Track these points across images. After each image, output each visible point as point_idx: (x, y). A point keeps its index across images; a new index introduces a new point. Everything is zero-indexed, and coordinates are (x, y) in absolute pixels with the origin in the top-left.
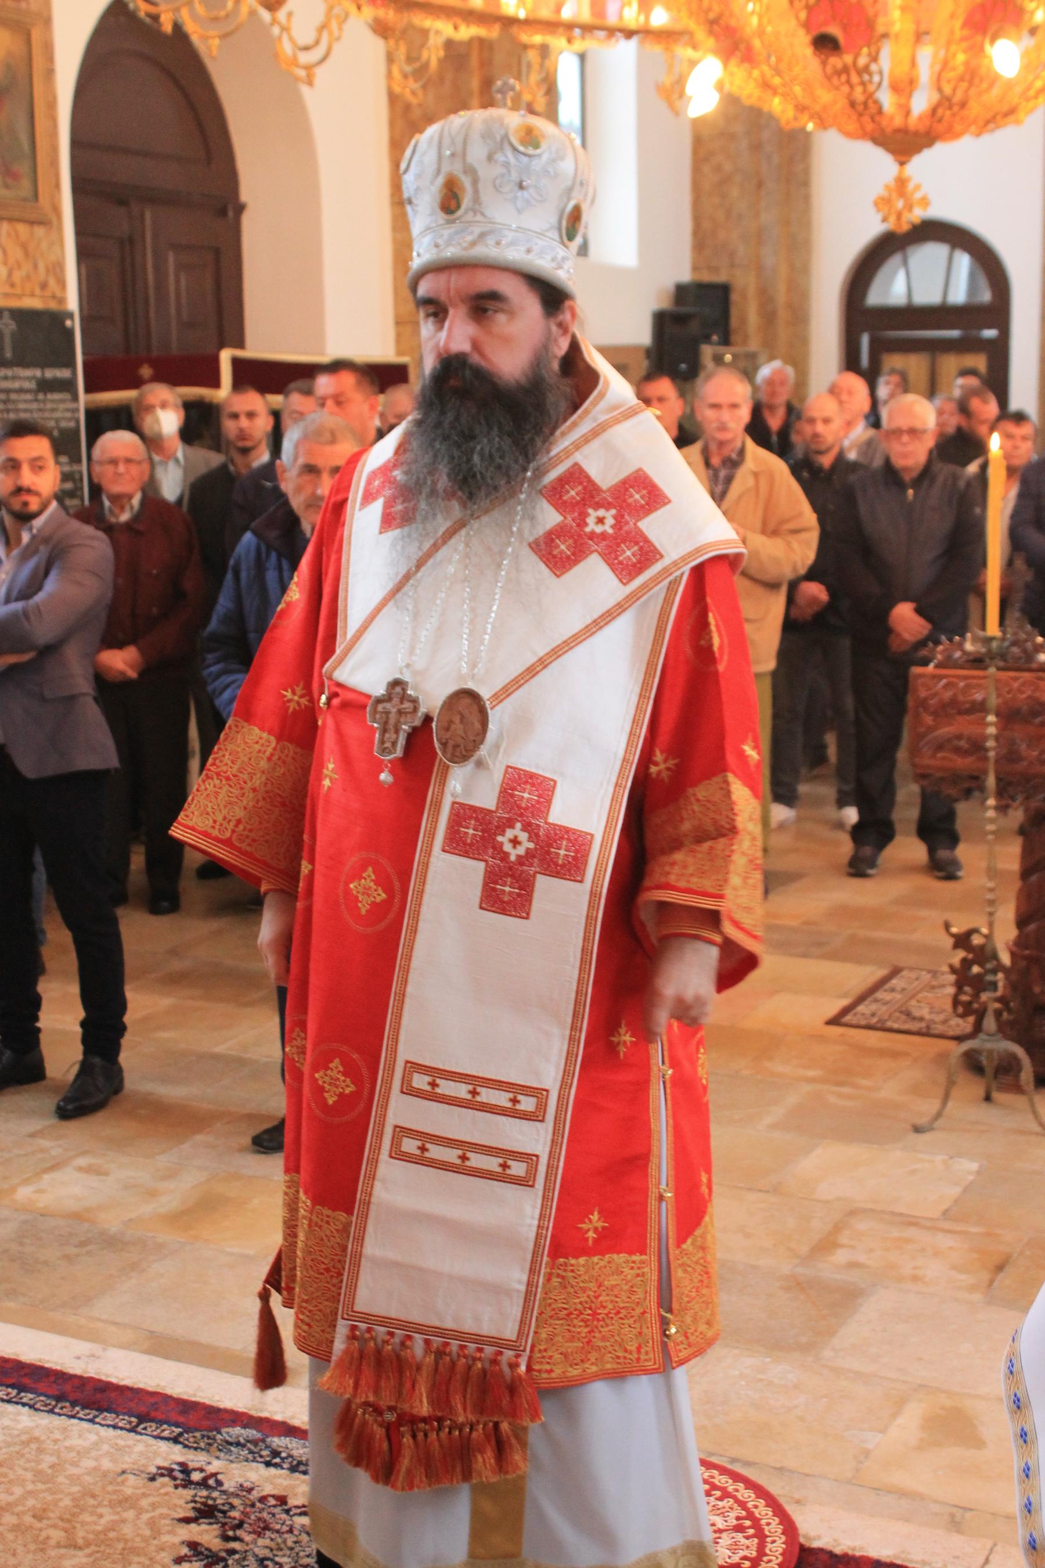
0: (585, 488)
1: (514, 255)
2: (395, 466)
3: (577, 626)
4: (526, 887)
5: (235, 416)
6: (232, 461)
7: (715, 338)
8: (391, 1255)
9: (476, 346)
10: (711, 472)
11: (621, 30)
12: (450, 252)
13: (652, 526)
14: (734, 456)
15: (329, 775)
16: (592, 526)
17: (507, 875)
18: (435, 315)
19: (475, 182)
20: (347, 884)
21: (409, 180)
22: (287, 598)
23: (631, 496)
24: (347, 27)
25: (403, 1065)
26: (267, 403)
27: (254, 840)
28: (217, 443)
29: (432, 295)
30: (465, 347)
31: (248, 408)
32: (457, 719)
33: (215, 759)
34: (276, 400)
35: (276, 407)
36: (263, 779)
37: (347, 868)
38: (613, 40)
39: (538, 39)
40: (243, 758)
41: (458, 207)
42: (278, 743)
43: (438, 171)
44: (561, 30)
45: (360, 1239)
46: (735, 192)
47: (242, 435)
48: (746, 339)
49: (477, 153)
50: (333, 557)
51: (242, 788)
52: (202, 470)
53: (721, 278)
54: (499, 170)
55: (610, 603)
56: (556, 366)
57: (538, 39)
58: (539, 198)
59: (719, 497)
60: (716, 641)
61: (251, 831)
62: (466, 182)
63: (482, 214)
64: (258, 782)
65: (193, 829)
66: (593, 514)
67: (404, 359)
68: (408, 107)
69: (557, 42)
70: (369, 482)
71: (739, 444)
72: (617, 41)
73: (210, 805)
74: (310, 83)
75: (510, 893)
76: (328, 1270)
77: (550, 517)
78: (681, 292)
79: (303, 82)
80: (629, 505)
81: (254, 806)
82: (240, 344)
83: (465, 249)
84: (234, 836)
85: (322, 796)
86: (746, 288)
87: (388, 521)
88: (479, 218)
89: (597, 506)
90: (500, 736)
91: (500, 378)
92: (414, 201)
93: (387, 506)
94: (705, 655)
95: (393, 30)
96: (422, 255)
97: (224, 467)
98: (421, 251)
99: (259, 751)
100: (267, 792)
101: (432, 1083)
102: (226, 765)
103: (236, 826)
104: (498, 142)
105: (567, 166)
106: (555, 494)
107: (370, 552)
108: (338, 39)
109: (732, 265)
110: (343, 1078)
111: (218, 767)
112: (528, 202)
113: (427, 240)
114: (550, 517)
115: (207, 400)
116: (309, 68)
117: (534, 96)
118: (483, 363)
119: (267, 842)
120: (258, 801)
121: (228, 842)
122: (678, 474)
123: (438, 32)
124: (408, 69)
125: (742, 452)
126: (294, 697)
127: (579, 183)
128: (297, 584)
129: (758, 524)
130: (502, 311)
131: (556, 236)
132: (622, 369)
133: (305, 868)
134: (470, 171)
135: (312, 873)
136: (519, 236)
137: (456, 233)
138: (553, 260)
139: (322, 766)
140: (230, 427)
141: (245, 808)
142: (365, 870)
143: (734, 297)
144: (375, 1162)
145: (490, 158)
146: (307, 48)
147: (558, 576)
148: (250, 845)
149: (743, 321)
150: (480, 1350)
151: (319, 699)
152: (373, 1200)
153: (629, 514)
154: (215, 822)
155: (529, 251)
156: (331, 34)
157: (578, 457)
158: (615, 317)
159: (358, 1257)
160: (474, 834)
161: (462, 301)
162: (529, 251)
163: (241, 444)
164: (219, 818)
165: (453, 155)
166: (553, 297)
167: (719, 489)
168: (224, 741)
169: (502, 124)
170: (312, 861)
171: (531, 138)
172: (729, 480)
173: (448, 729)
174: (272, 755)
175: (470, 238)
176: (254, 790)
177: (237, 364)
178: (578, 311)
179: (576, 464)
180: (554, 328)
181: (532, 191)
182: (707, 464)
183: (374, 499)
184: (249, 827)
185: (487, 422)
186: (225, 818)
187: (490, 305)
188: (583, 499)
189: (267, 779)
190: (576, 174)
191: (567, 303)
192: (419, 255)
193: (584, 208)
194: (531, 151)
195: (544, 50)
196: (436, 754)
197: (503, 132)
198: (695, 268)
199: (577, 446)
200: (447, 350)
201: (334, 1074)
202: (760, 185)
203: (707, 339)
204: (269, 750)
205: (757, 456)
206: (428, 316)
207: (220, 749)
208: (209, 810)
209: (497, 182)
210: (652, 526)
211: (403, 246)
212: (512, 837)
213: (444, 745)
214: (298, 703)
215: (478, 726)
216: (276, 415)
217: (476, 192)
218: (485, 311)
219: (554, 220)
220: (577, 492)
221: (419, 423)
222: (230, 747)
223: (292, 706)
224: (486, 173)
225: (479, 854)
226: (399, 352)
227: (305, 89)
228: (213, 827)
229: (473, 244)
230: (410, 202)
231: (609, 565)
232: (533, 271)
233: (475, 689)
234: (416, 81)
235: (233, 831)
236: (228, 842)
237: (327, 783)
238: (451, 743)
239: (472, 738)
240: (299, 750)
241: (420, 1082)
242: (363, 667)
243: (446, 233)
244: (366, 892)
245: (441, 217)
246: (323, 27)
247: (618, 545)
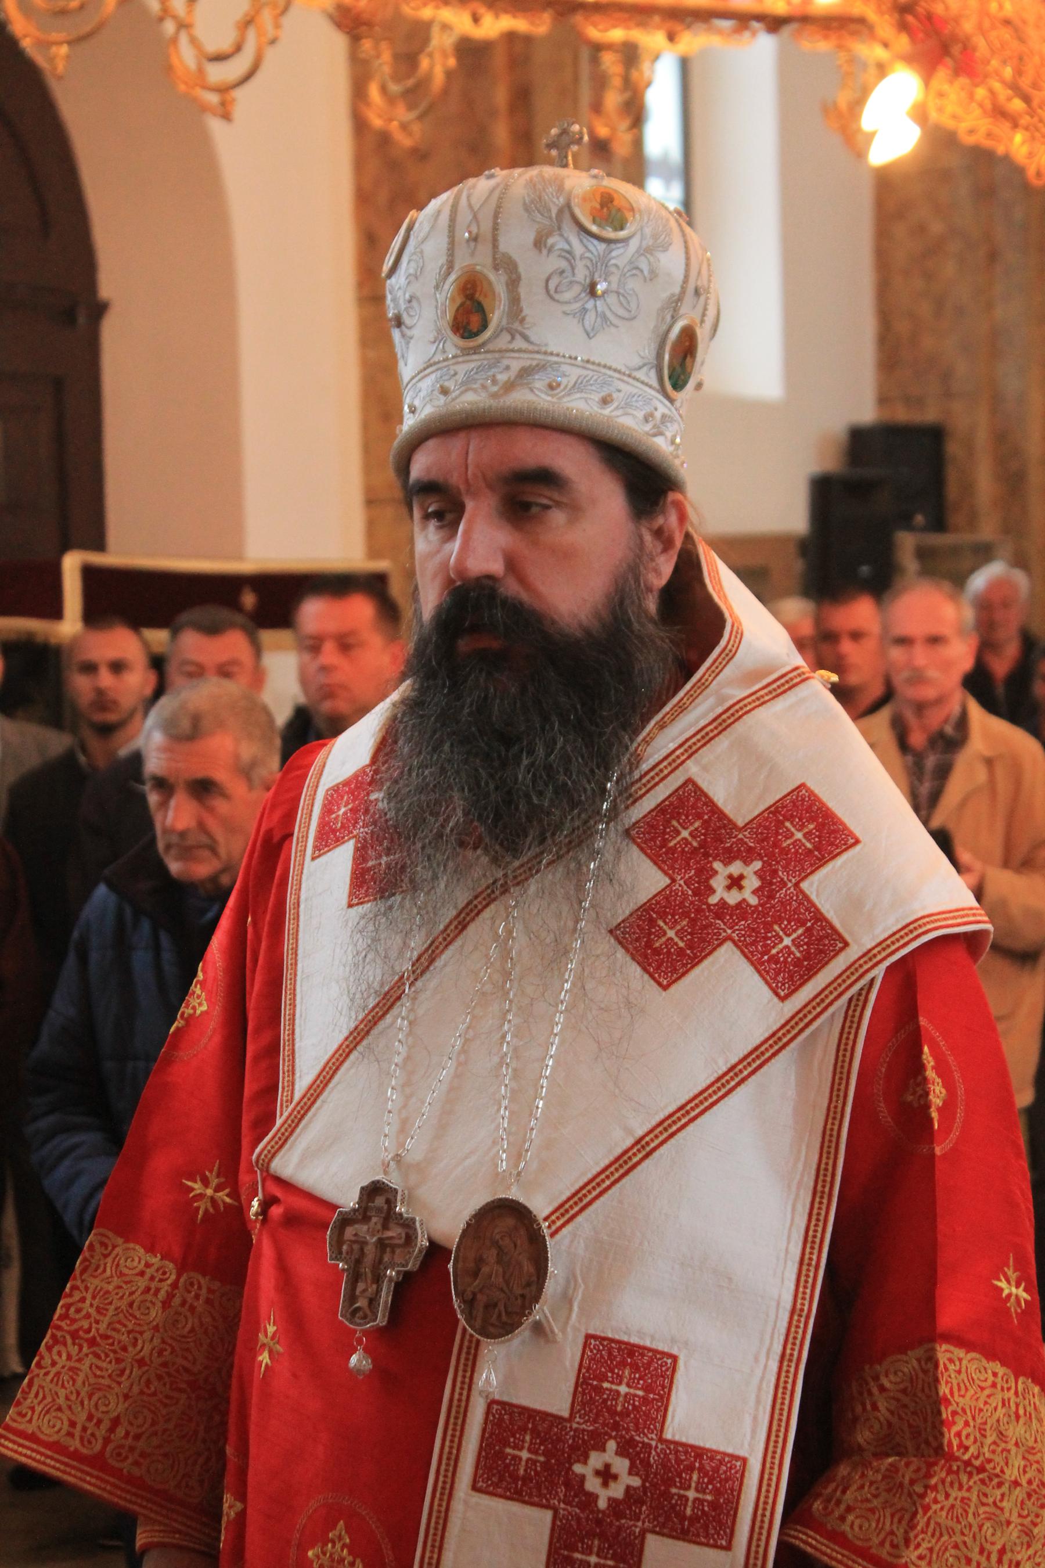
0: (706, 824)
1: (582, 406)
2: (374, 783)
3: (702, 1079)
5: (90, 668)
6: (84, 749)
7: (919, 519)
9: (512, 564)
10: (910, 758)
11: (760, 18)
12: (471, 400)
13: (825, 888)
14: (949, 730)
15: (269, 1347)
16: (720, 892)
17: (591, 1535)
18: (439, 515)
19: (514, 283)
20: (303, 1549)
21: (397, 287)
22: (185, 1010)
23: (789, 835)
24: (286, 21)
26: (146, 644)
27: (143, 1455)
28: (57, 711)
29: (434, 475)
30: (496, 567)
31: (112, 654)
32: (491, 1255)
33: (68, 1307)
34: (158, 637)
35: (157, 649)
36: (156, 1341)
37: (302, 1520)
38: (747, 34)
39: (617, 34)
40: (117, 1303)
41: (484, 325)
42: (179, 1276)
43: (450, 266)
44: (657, 19)
46: (949, 269)
47: (102, 701)
48: (972, 521)
49: (516, 240)
50: (254, 862)
51: (118, 1361)
52: (32, 761)
53: (929, 415)
54: (554, 263)
55: (758, 1033)
56: (651, 605)
57: (617, 34)
58: (621, 312)
59: (924, 805)
60: (937, 1094)
61: (137, 1437)
62: (498, 282)
63: (526, 338)
64: (147, 1348)
65: (32, 1438)
66: (722, 872)
67: (382, 565)
68: (384, 139)
69: (652, 39)
70: (328, 809)
71: (956, 709)
72: (754, 34)
73: (62, 1393)
74: (227, 116)
77: (646, 879)
78: (860, 441)
79: (215, 114)
80: (785, 851)
81: (142, 1393)
82: (99, 545)
83: (494, 396)
84: (109, 1449)
85: (256, 1384)
86: (971, 427)
87: (364, 883)
88: (519, 343)
89: (729, 858)
90: (571, 1279)
91: (553, 622)
92: (406, 318)
93: (360, 855)
94: (915, 1119)
95: (369, 24)
96: (420, 404)
97: (68, 760)
98: (417, 403)
99: (147, 1290)
100: (165, 1365)
102: (88, 1316)
103: (112, 1430)
104: (556, 219)
105: (672, 261)
106: (653, 838)
107: (330, 932)
108: (273, 42)
109: (948, 394)
111: (74, 1321)
112: (604, 318)
113: (427, 384)
114: (646, 879)
115: (40, 639)
116: (224, 90)
117: (614, 129)
118: (525, 596)
119: (166, 1455)
120: (148, 1383)
121: (97, 1462)
122: (860, 777)
123: (445, 27)
124: (394, 88)
125: (963, 723)
126: (206, 1192)
127: (695, 290)
128: (203, 983)
129: (998, 852)
130: (558, 504)
131: (654, 382)
132: (755, 578)
133: (230, 1506)
134: (507, 265)
135: (242, 1515)
136: (589, 369)
137: (479, 370)
138: (646, 419)
139: (256, 1327)
140: (81, 685)
141: (126, 1397)
142: (334, 1527)
143: (953, 448)
145: (539, 243)
146: (219, 58)
147: (665, 988)
148: (136, 1463)
149: (968, 488)
151: (250, 1206)
153: (785, 868)
154: (73, 1424)
155: (605, 401)
156: (260, 34)
157: (692, 769)
158: (748, 480)
160: (529, 1456)
161: (490, 487)
162: (605, 401)
163: (99, 717)
164: (81, 1417)
165: (475, 239)
166: (647, 483)
167: (925, 788)
168: (84, 1271)
169: (560, 188)
170: (242, 1496)
171: (610, 212)
172: (943, 772)
173: (475, 1274)
174: (170, 1296)
175: (502, 378)
176: (141, 1362)
177: (89, 573)
178: (690, 511)
179: (689, 781)
180: (648, 538)
181: (612, 299)
182: (903, 745)
183: (339, 841)
184: (133, 1431)
185: (533, 713)
186: (90, 1417)
187: (541, 495)
188: (703, 845)
189: (163, 1342)
190: (686, 277)
191: (672, 496)
192: (413, 411)
193: (702, 334)
194: (609, 233)
195: (630, 54)
196: (457, 1320)
197: (562, 201)
198: (883, 400)
199: (691, 748)
200: (461, 572)
202: (993, 256)
203: (905, 521)
204: (165, 1287)
205: (989, 731)
206: (427, 517)
207: (74, 1288)
208: (61, 1401)
209: (552, 285)
210: (825, 888)
211: (380, 392)
213: (470, 1304)
214: (213, 1200)
215: (528, 1267)
216: (158, 663)
217: (515, 301)
218: (526, 506)
219: (649, 353)
220: (690, 832)
221: (412, 706)
222: (94, 1283)
223: (202, 1206)
224: (535, 268)
226: (373, 553)
227: (215, 126)
228: (70, 1435)
229: (509, 387)
230: (399, 322)
231: (752, 964)
232: (614, 435)
233: (521, 1200)
234: (411, 107)
235: (107, 1441)
236: (97, 1462)
237: (264, 1358)
238: (482, 1299)
239: (518, 1291)
240: (216, 1285)
242: (325, 1157)
243: (462, 369)
245: (453, 344)
246: (247, 23)
247: (768, 927)
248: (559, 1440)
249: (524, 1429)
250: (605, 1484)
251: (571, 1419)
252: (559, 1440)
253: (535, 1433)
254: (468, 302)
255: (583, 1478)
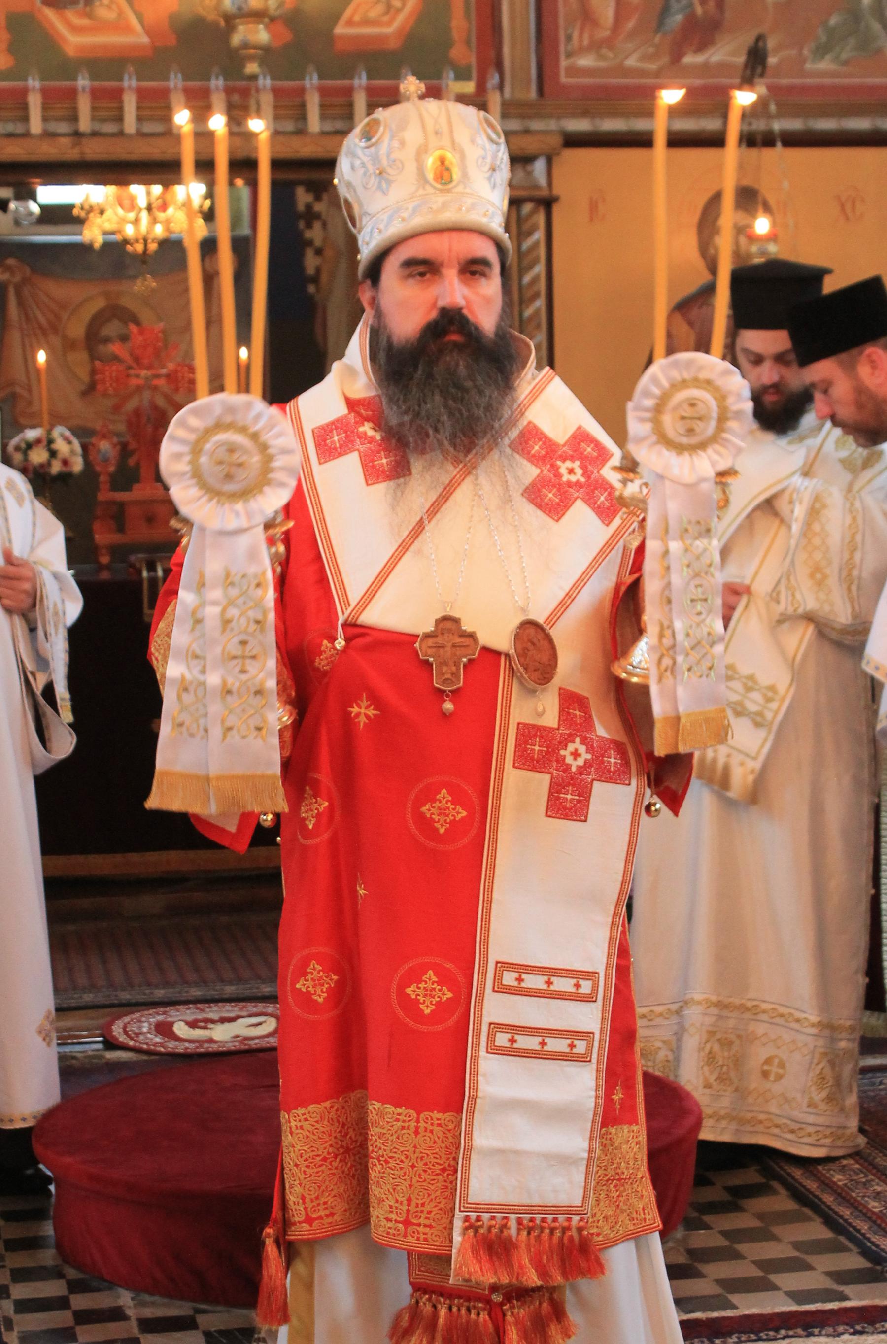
4: (585, 794)
8: (495, 1143)
17: (569, 784)
25: (487, 1026)
45: (469, 1134)
75: (572, 800)
76: (444, 1170)
101: (518, 978)
110: (453, 806)
144: (476, 1059)
150: (555, 1220)
152: (479, 1094)
154: (403, 1128)
159: (469, 1149)
201: (429, 985)
212: (572, 757)
223: (364, 703)
225: (545, 767)
235: (419, 1225)
241: (509, 979)
244: (429, 993)
248: (553, 739)
249: (535, 736)
250: (575, 759)
251: (558, 729)
252: (553, 739)
253: (541, 737)
254: (377, 398)
255: (565, 757)
